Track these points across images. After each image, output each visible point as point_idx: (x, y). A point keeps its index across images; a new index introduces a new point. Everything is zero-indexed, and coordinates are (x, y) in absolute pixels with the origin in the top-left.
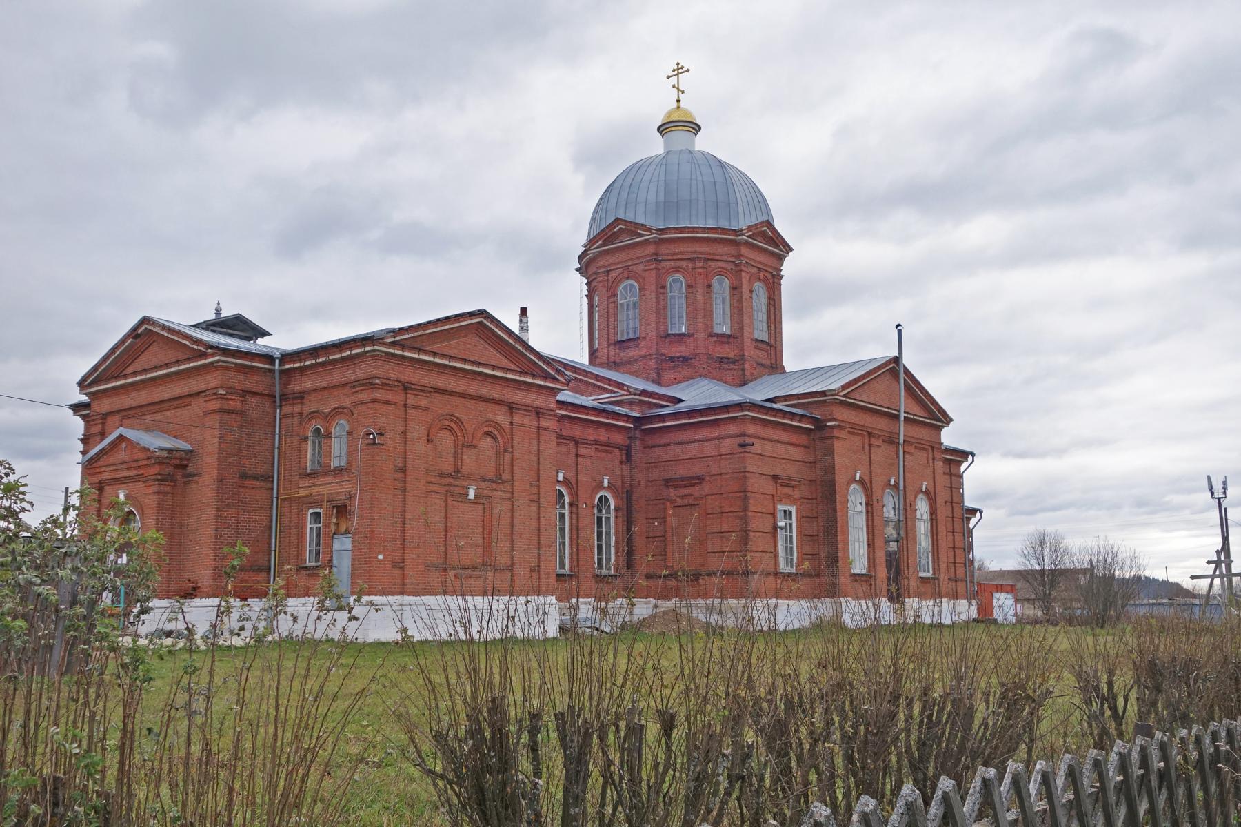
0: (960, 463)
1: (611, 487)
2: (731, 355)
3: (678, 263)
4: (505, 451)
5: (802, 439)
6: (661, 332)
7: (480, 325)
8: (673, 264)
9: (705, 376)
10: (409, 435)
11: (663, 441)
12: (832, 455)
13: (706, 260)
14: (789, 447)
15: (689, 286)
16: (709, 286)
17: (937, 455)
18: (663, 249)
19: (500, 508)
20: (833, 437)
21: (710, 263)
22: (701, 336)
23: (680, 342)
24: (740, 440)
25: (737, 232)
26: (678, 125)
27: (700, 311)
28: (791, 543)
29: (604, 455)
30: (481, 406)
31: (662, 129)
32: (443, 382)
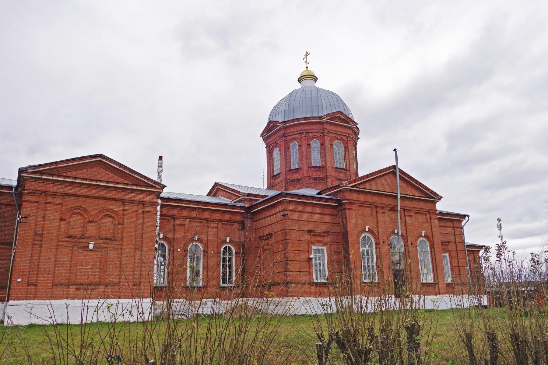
0: (461, 221)
1: (231, 242)
2: (321, 176)
3: (294, 136)
4: (119, 224)
5: (332, 211)
6: (288, 169)
7: (100, 162)
8: (292, 137)
9: (307, 187)
10: (47, 218)
11: (264, 216)
12: (346, 218)
13: (307, 133)
14: (321, 216)
15: (300, 146)
16: (309, 145)
17: (432, 216)
18: (288, 131)
19: (112, 254)
20: (345, 209)
21: (309, 134)
22: (305, 169)
23: (296, 172)
24: (283, 213)
25: (320, 118)
26: (308, 77)
27: (306, 156)
29: (227, 226)
30: (102, 202)
31: (300, 80)
32: (73, 191)
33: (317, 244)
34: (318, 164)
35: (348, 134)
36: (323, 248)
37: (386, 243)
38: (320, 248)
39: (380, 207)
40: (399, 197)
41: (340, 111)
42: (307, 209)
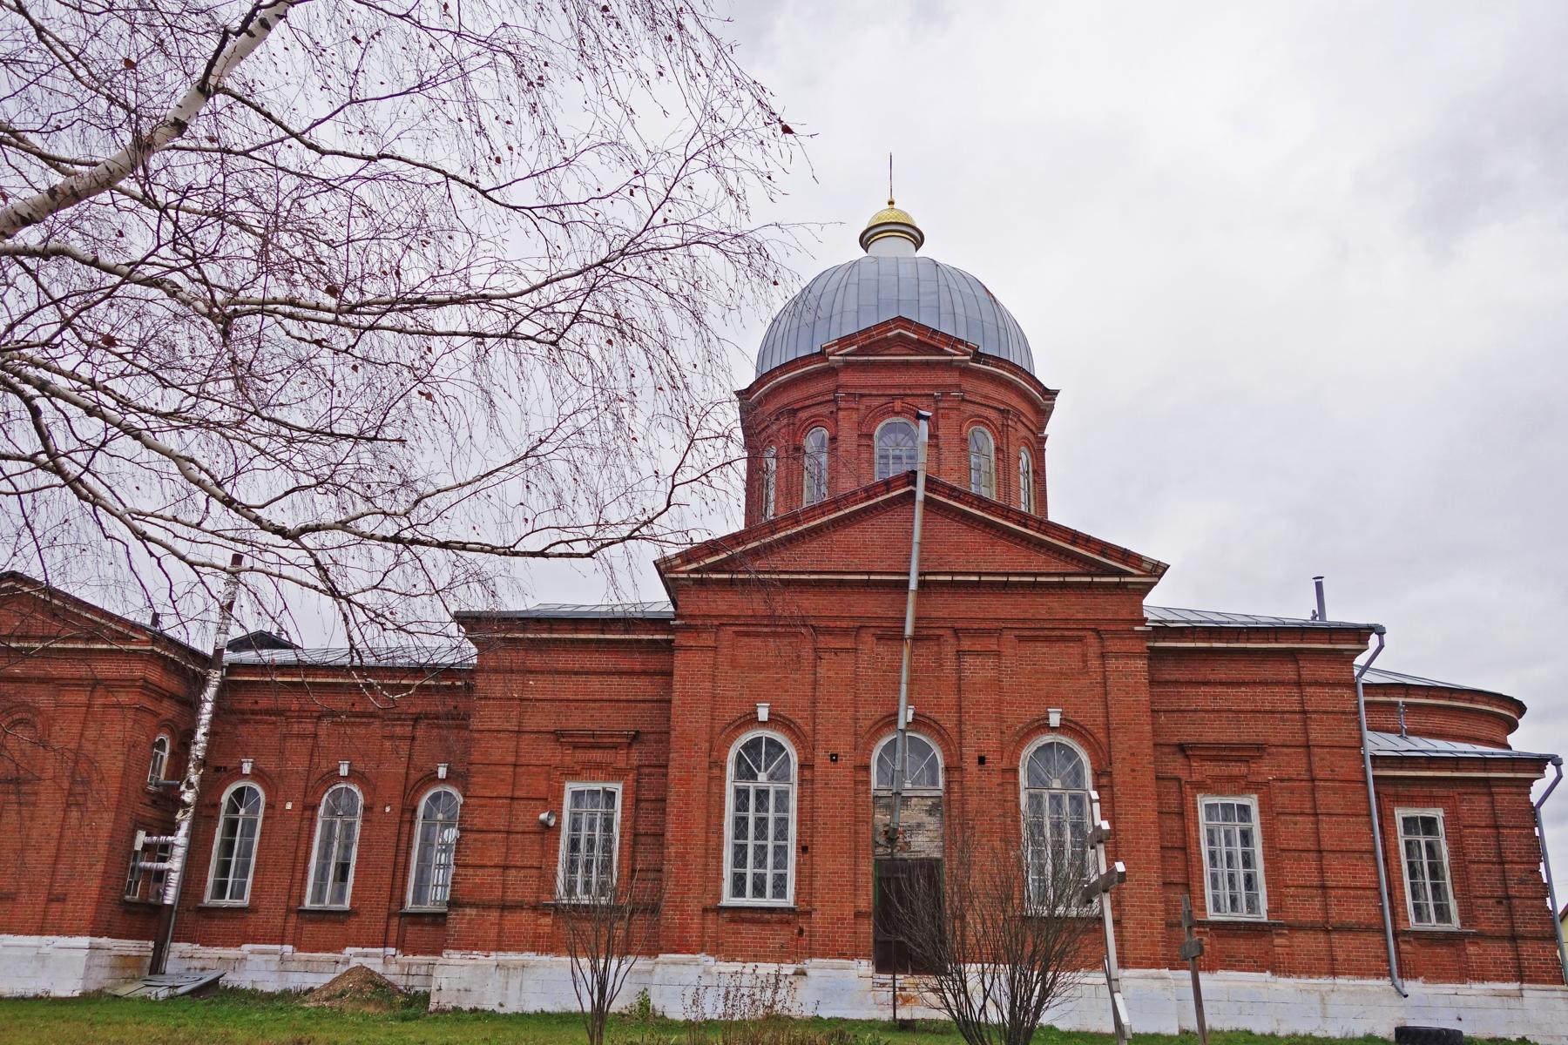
14: (616, 680)
25: (822, 354)
33: (586, 773)
35: (936, 387)
37: (843, 761)
38: (598, 786)
39: (829, 631)
40: (913, 586)
41: (900, 318)
42: (563, 660)
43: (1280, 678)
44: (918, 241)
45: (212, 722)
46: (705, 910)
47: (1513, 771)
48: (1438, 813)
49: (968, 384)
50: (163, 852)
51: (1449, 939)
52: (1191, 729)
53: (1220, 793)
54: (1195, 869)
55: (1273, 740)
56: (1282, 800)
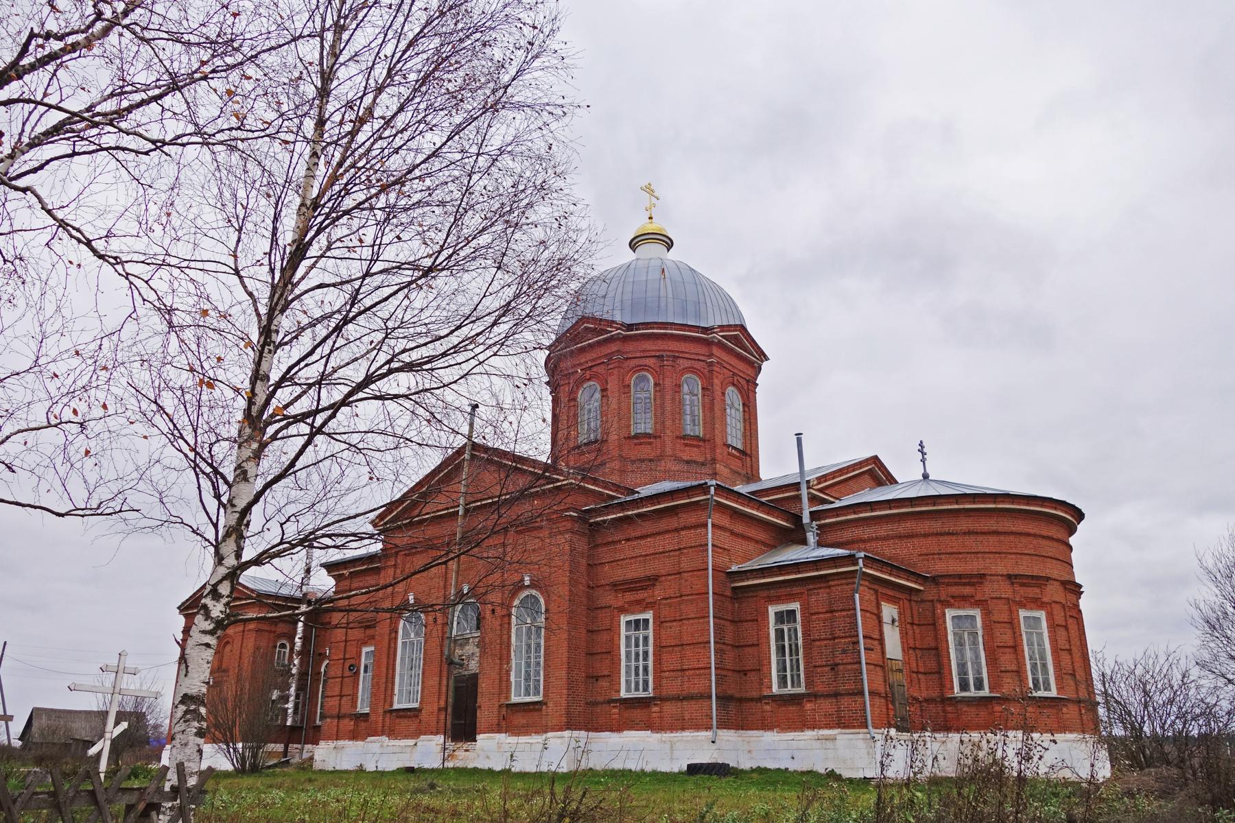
8: (637, 362)
21: (681, 361)
25: (705, 330)
28: (798, 669)
31: (633, 245)
34: (699, 431)
36: (971, 612)
43: (669, 528)
44: (669, 245)
45: (304, 631)
46: (385, 712)
47: (836, 567)
48: (795, 606)
49: (630, 347)
50: (285, 699)
51: (795, 699)
52: (620, 572)
53: (633, 613)
54: (946, 661)
55: (663, 572)
56: (665, 612)
